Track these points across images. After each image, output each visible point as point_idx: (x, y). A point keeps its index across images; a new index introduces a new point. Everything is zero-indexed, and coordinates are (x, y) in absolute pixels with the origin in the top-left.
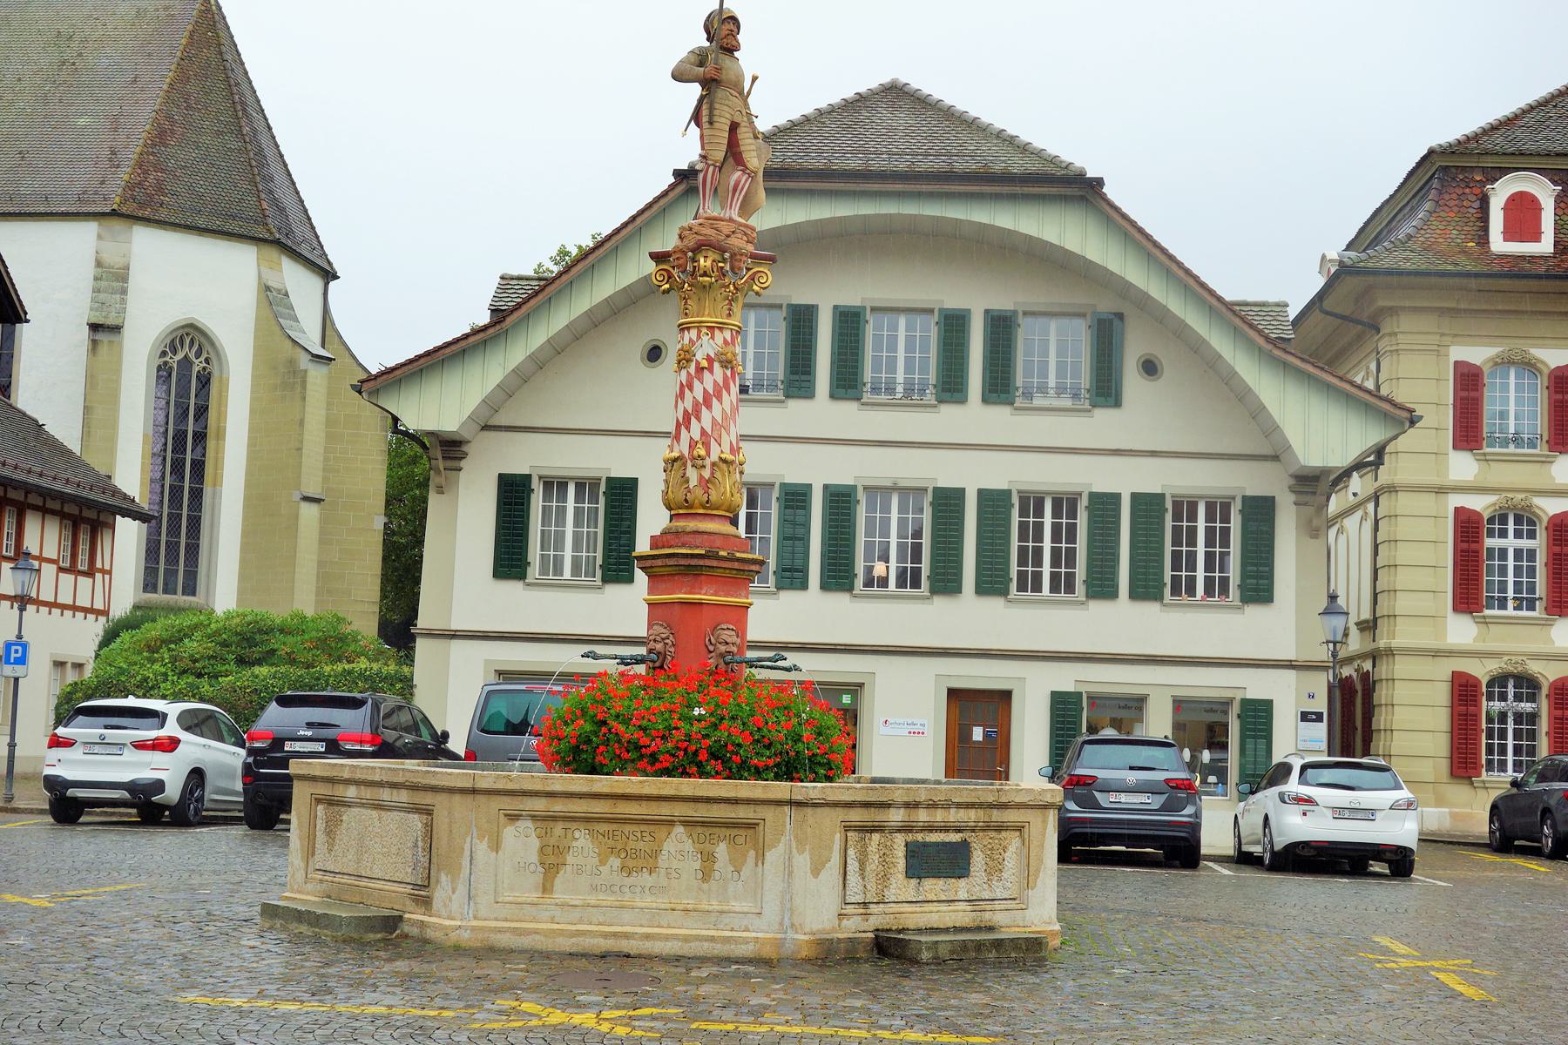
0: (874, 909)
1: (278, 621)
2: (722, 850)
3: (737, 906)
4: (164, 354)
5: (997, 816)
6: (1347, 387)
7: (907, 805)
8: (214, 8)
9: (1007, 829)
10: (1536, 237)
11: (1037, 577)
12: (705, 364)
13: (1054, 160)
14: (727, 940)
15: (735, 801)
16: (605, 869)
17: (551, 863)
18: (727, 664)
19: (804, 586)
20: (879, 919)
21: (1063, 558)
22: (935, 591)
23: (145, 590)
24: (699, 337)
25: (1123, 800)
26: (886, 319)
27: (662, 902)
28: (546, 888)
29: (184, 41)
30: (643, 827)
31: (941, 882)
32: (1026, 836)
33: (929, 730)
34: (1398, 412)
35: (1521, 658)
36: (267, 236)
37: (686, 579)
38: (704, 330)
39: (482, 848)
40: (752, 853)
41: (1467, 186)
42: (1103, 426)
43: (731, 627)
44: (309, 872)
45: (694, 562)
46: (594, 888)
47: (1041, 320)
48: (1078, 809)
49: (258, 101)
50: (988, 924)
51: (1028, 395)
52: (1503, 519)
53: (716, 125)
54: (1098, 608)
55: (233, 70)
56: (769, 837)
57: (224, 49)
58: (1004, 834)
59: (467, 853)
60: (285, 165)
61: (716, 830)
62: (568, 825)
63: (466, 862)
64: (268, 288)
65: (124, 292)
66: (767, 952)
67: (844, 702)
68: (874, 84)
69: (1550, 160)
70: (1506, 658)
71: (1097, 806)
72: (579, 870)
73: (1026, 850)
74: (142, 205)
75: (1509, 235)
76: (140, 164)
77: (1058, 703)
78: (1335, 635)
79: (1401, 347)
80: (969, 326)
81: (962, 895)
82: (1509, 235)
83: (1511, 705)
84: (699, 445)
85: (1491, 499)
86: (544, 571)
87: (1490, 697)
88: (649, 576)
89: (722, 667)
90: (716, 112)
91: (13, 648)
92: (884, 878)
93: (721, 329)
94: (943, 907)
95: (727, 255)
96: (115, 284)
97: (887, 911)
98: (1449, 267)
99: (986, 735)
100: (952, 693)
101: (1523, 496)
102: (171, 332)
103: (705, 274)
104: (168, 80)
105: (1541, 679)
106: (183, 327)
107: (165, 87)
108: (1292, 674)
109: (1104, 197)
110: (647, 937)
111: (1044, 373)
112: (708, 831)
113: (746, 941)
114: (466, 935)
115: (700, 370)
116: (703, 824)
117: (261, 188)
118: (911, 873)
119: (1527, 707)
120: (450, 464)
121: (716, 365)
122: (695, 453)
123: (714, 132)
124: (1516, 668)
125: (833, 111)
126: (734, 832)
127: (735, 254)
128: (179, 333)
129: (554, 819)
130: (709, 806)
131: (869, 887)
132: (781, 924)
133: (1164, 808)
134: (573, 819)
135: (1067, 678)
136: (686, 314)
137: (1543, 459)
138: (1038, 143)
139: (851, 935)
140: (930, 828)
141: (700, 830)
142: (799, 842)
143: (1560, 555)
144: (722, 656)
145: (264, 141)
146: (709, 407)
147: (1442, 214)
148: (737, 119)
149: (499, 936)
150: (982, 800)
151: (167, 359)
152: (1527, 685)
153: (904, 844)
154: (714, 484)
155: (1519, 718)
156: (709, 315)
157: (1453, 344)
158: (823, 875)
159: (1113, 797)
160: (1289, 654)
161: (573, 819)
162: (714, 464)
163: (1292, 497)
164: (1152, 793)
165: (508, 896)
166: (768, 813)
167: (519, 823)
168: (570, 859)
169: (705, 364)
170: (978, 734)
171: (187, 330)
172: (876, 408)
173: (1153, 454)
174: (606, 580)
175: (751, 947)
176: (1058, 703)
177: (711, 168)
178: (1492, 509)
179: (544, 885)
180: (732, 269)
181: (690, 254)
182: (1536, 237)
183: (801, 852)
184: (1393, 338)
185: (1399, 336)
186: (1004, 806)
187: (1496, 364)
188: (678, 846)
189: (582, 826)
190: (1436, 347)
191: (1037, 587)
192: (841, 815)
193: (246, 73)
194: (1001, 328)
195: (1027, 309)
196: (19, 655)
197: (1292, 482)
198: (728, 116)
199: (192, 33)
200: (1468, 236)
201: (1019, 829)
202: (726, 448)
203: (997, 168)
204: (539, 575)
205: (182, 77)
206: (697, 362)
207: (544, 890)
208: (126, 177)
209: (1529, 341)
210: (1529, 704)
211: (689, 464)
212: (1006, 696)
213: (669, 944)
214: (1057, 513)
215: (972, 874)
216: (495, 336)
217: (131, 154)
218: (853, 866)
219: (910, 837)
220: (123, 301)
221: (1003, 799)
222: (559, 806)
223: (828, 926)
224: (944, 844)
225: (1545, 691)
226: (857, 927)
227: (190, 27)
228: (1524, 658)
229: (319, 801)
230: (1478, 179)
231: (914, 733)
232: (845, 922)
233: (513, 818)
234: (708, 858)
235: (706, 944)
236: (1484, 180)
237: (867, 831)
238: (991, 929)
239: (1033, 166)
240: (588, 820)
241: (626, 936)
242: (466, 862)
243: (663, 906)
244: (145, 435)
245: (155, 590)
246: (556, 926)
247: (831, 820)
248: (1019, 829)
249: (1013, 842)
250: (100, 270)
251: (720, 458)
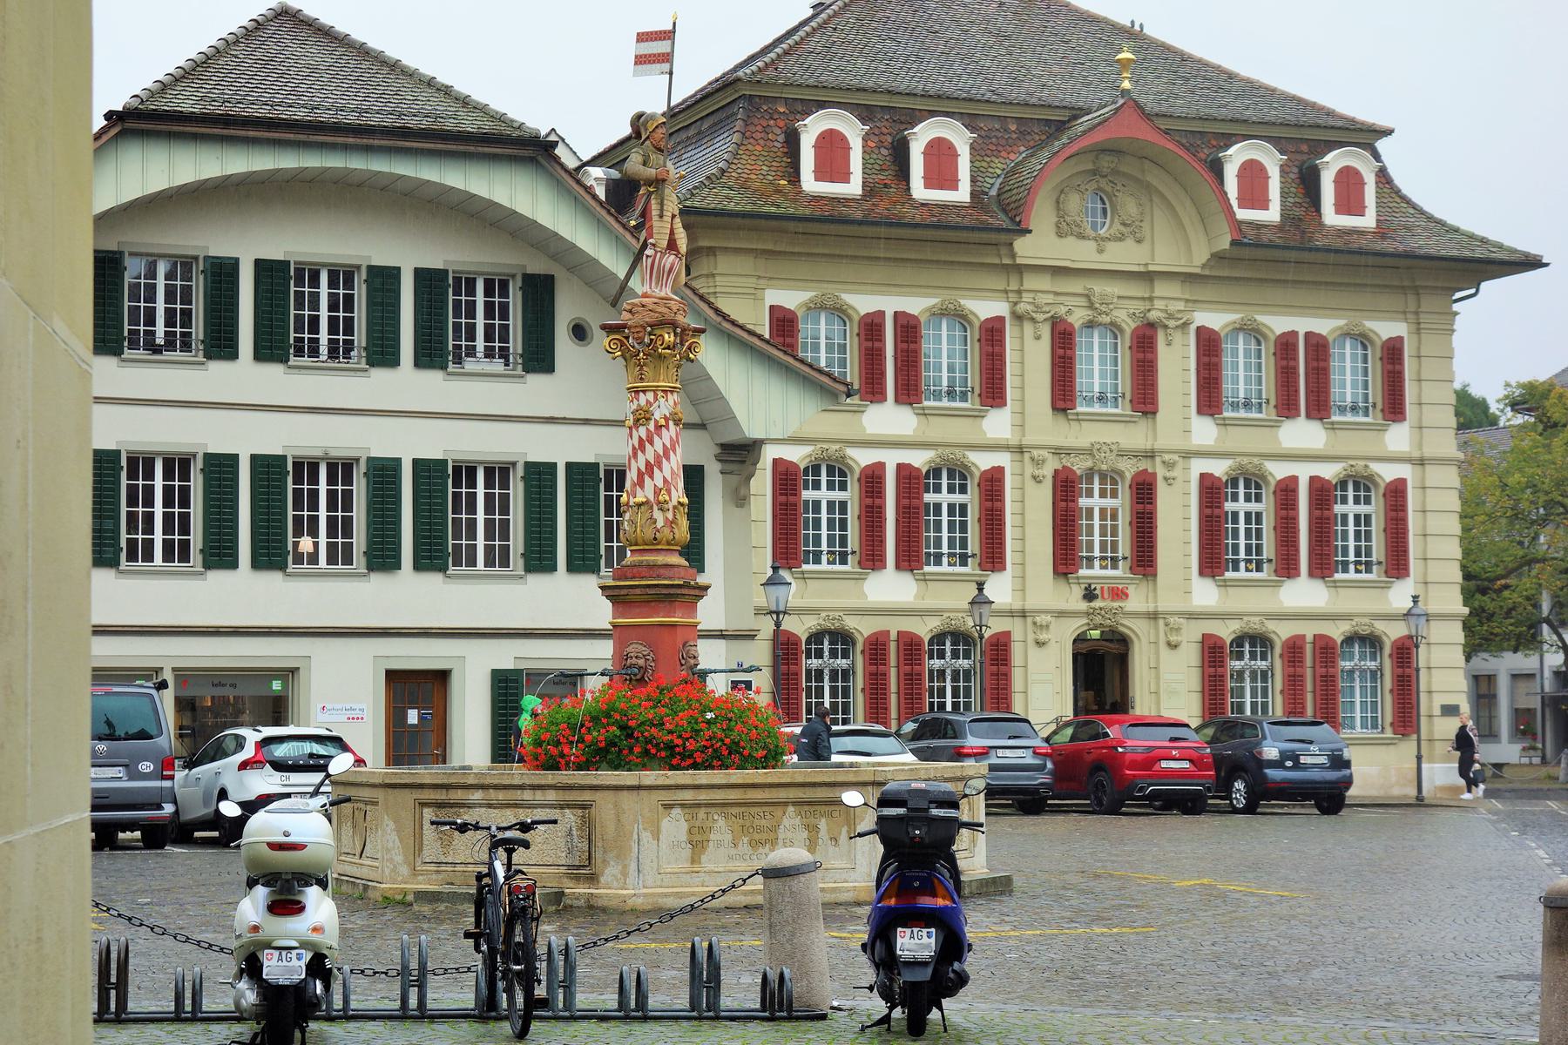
2: (823, 824)
6: (791, 360)
10: (845, 177)
12: (663, 422)
13: (501, 118)
14: (834, 890)
17: (697, 844)
19: (234, 565)
21: (495, 530)
24: (656, 399)
30: (765, 809)
33: (368, 716)
34: (837, 386)
35: (837, 614)
37: (661, 605)
38: (660, 394)
39: (646, 836)
41: (772, 118)
42: (533, 393)
44: (417, 864)
45: (672, 591)
51: (458, 360)
52: (816, 470)
54: (537, 581)
61: (818, 808)
62: (709, 810)
67: (274, 688)
69: (849, 95)
70: (823, 614)
72: (719, 844)
75: (820, 175)
77: (500, 681)
78: (777, 605)
79: (718, 289)
82: (820, 175)
83: (826, 662)
85: (806, 450)
87: (809, 657)
90: (665, 207)
93: (644, 392)
95: (679, 330)
98: (773, 209)
99: (421, 718)
100: (392, 675)
101: (837, 447)
105: (856, 634)
108: (722, 642)
112: (812, 809)
114: (640, 900)
115: (658, 427)
116: (810, 803)
119: (842, 663)
121: (671, 423)
122: (660, 498)
124: (833, 624)
125: (238, 41)
127: (685, 330)
129: (699, 805)
130: (814, 789)
135: (507, 656)
136: (641, 379)
137: (856, 409)
138: (478, 96)
141: (806, 808)
143: (872, 507)
147: (750, 147)
152: (842, 639)
154: (677, 524)
155: (834, 675)
156: (663, 380)
157: (769, 287)
163: (717, 466)
166: (598, 796)
169: (663, 422)
170: (413, 717)
172: (303, 371)
173: (587, 422)
176: (500, 681)
177: (659, 254)
178: (808, 460)
179: (692, 858)
181: (649, 329)
182: (845, 177)
184: (711, 280)
185: (718, 278)
187: (809, 309)
189: (719, 810)
190: (752, 291)
197: (718, 450)
200: (779, 173)
203: (450, 125)
206: (656, 421)
207: (693, 862)
209: (839, 286)
210: (844, 661)
211: (655, 507)
212: (442, 677)
222: (703, 796)
225: (859, 647)
228: (841, 614)
229: (423, 805)
230: (782, 110)
231: (353, 718)
233: (668, 807)
236: (787, 112)
239: (488, 126)
251: (679, 503)
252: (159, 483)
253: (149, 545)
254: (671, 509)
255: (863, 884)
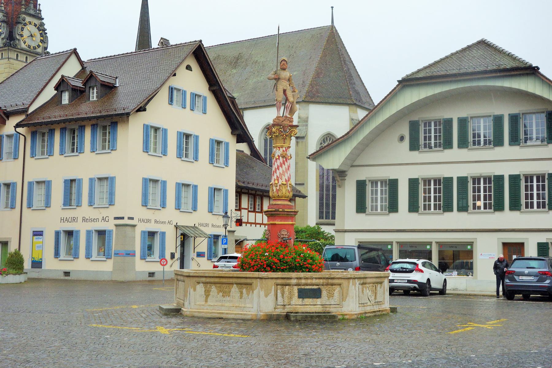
0: (287, 306)
1: (300, 229)
2: (244, 291)
3: (248, 305)
4: (321, 143)
5: (330, 281)
7: (297, 278)
8: (334, 31)
9: (335, 285)
11: (532, 203)
12: (277, 157)
14: (245, 314)
15: (246, 278)
16: (219, 296)
18: (284, 240)
20: (288, 309)
22: (495, 210)
23: (320, 218)
25: (524, 279)
26: (476, 120)
27: (231, 304)
28: (206, 301)
29: (325, 43)
30: (227, 285)
31: (311, 299)
32: (342, 287)
36: (352, 103)
38: (277, 148)
39: (192, 290)
40: (251, 291)
43: (285, 230)
46: (216, 301)
47: (530, 115)
48: (509, 282)
49: (350, 59)
50: (328, 311)
51: (526, 142)
53: (278, 91)
55: (341, 50)
56: (254, 287)
57: (337, 44)
58: (334, 286)
59: (189, 292)
60: (360, 78)
62: (211, 285)
63: (188, 295)
64: (352, 119)
65: (307, 125)
66: (254, 317)
67: (468, 248)
68: (475, 41)
71: (515, 281)
72: (213, 296)
73: (342, 291)
74: (312, 97)
76: (311, 85)
77: (540, 246)
80: (503, 120)
81: (319, 303)
84: (276, 180)
86: (425, 209)
88: (268, 217)
89: (283, 242)
91: (224, 240)
92: (291, 298)
93: (282, 147)
94: (312, 306)
96: (304, 123)
97: (291, 307)
100: (505, 244)
102: (324, 136)
103: (274, 133)
104: (320, 57)
106: (327, 134)
107: (319, 59)
109: (540, 73)
110: (227, 314)
111: (532, 134)
113: (249, 315)
114: (188, 313)
117: (350, 87)
118: (300, 297)
120: (342, 178)
121: (281, 158)
123: (278, 93)
125: (457, 53)
126: (248, 286)
128: (326, 136)
129: (208, 283)
131: (285, 301)
132: (258, 310)
133: (538, 281)
134: (212, 283)
139: (278, 314)
140: (307, 285)
141: (240, 285)
142: (262, 289)
144: (282, 238)
145: (352, 72)
146: (279, 169)
148: (285, 88)
149: (195, 313)
150: (324, 277)
151: (322, 145)
153: (297, 289)
158: (269, 297)
159: (521, 278)
160: (346, 234)
161: (212, 283)
162: (280, 185)
164: (534, 276)
165: (198, 303)
167: (200, 284)
168: (211, 293)
171: (328, 135)
172: (473, 150)
174: (390, 212)
175: (250, 316)
177: (278, 103)
180: (284, 130)
183: (262, 291)
186: (366, 278)
188: (235, 289)
189: (214, 285)
191: (532, 207)
192: (274, 281)
193: (346, 50)
194: (514, 119)
195: (524, 112)
196: (225, 242)
198: (281, 88)
199: (327, 41)
201: (340, 285)
202: (284, 180)
204: (371, 211)
205: (324, 55)
207: (206, 302)
208: (307, 89)
213: (232, 315)
214: (538, 181)
215: (322, 297)
216: (347, 139)
217: (308, 82)
218: (279, 295)
219: (299, 287)
220: (307, 129)
221: (332, 276)
222: (208, 280)
223: (270, 311)
224: (312, 289)
226: (280, 311)
227: (327, 39)
232: (276, 310)
233: (199, 283)
234: (241, 293)
235: (240, 315)
237: (284, 285)
238: (329, 313)
240: (215, 283)
241: (222, 313)
242: (188, 295)
243: (231, 306)
244: (316, 170)
245: (323, 218)
246: (208, 311)
247: (272, 282)
248: (340, 285)
249: (337, 289)
250: (299, 119)
252: (482, 185)
253: (430, 205)
254: (278, 186)
255: (254, 313)
